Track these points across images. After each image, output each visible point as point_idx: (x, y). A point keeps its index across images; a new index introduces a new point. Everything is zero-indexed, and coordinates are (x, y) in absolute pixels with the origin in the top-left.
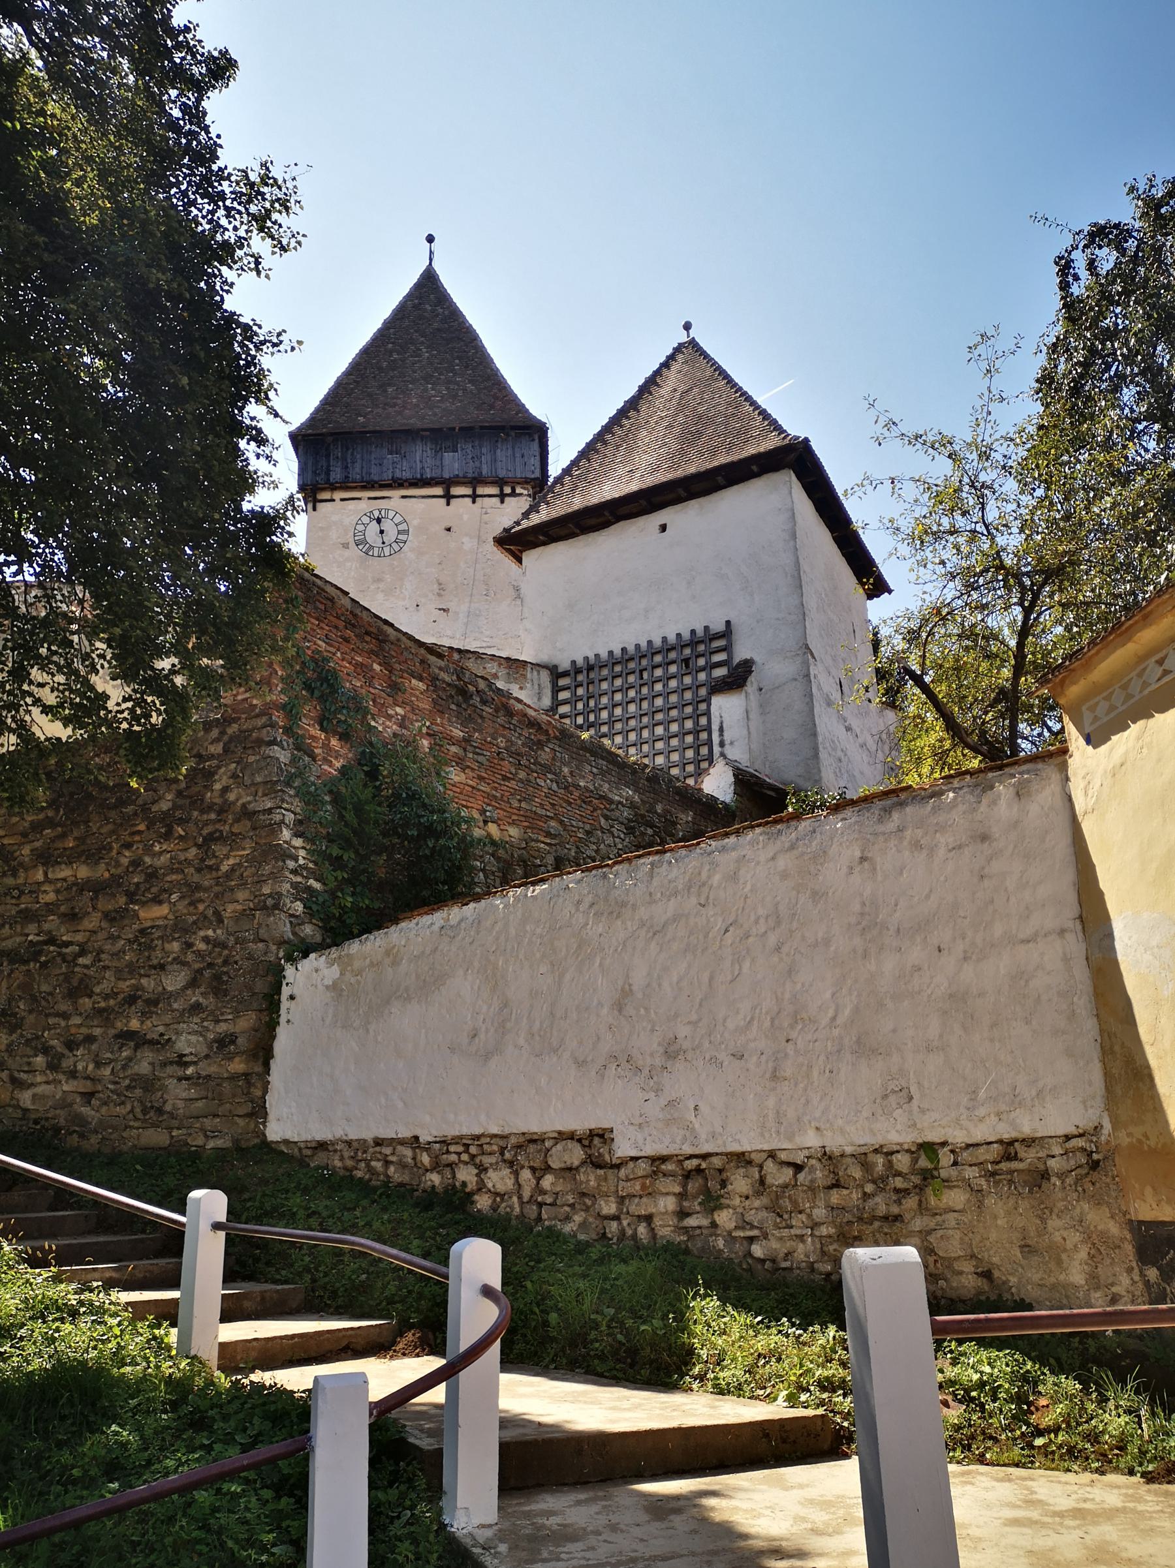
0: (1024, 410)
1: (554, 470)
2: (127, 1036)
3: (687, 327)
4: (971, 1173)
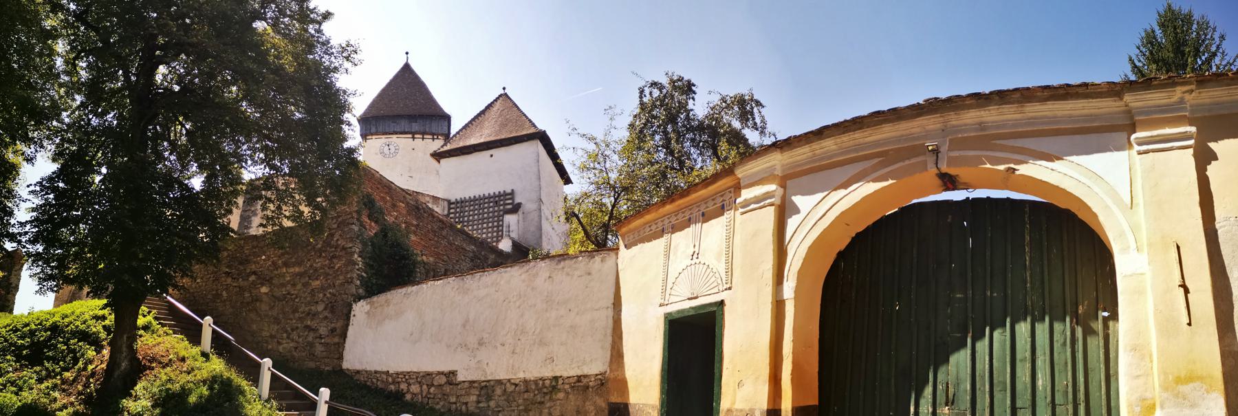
0: (622, 134)
1: (453, 132)
2: (307, 327)
4: (567, 386)
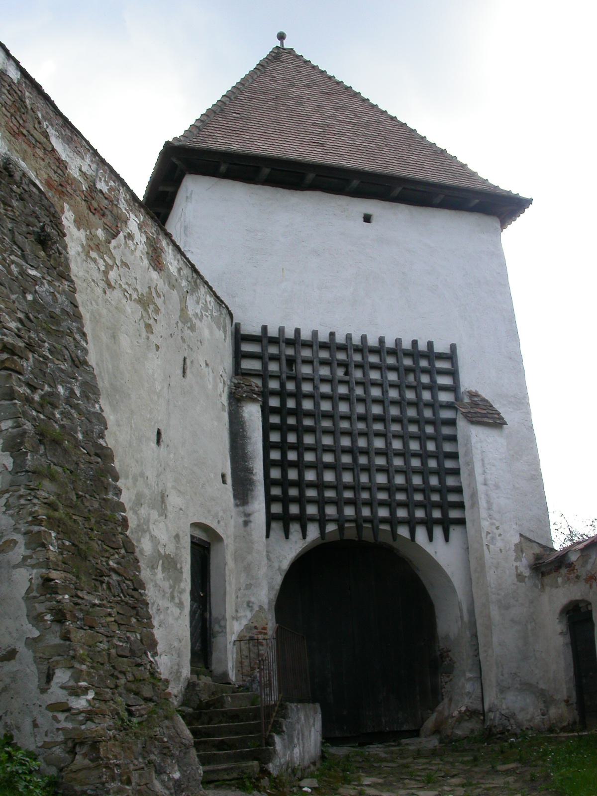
3: (281, 37)
